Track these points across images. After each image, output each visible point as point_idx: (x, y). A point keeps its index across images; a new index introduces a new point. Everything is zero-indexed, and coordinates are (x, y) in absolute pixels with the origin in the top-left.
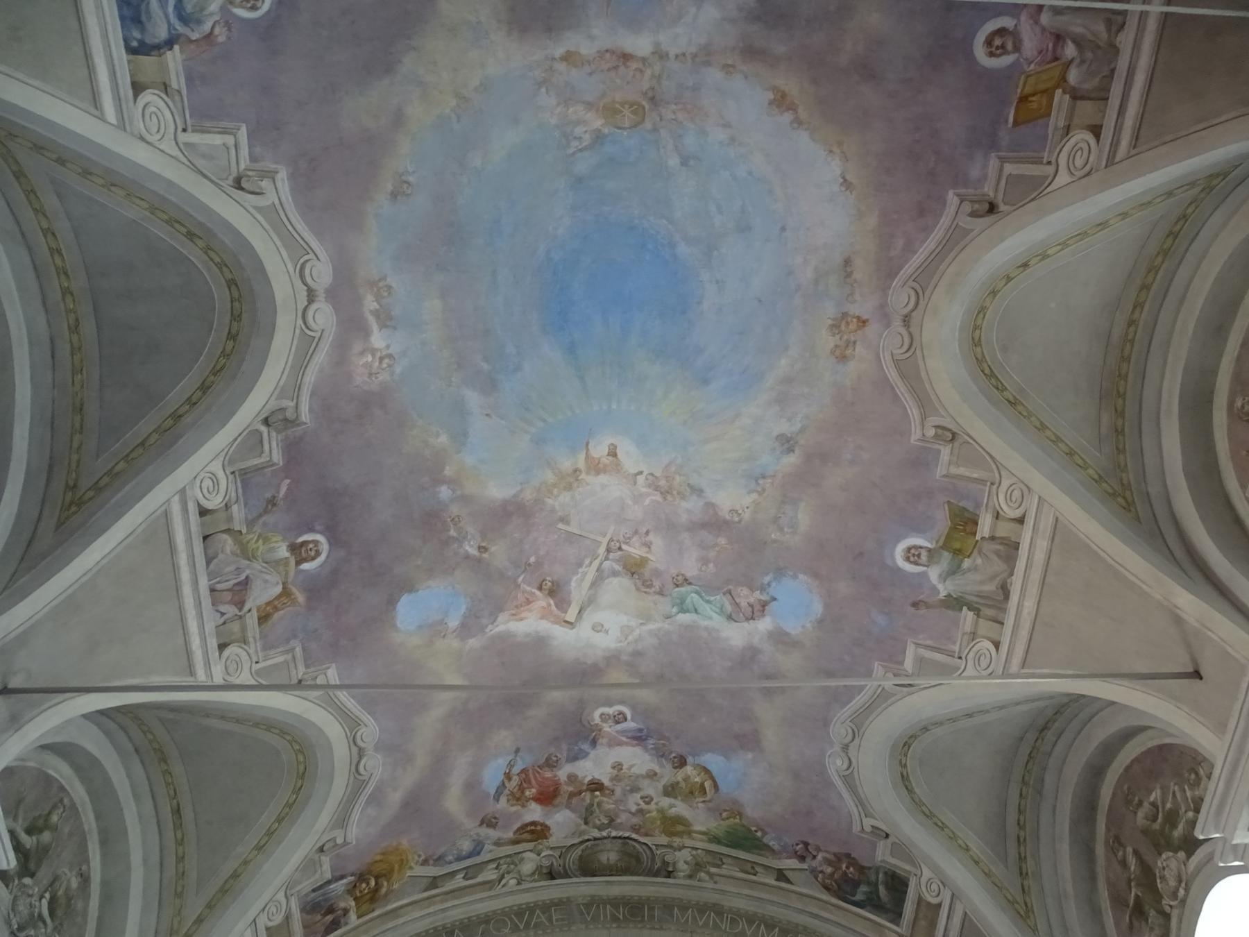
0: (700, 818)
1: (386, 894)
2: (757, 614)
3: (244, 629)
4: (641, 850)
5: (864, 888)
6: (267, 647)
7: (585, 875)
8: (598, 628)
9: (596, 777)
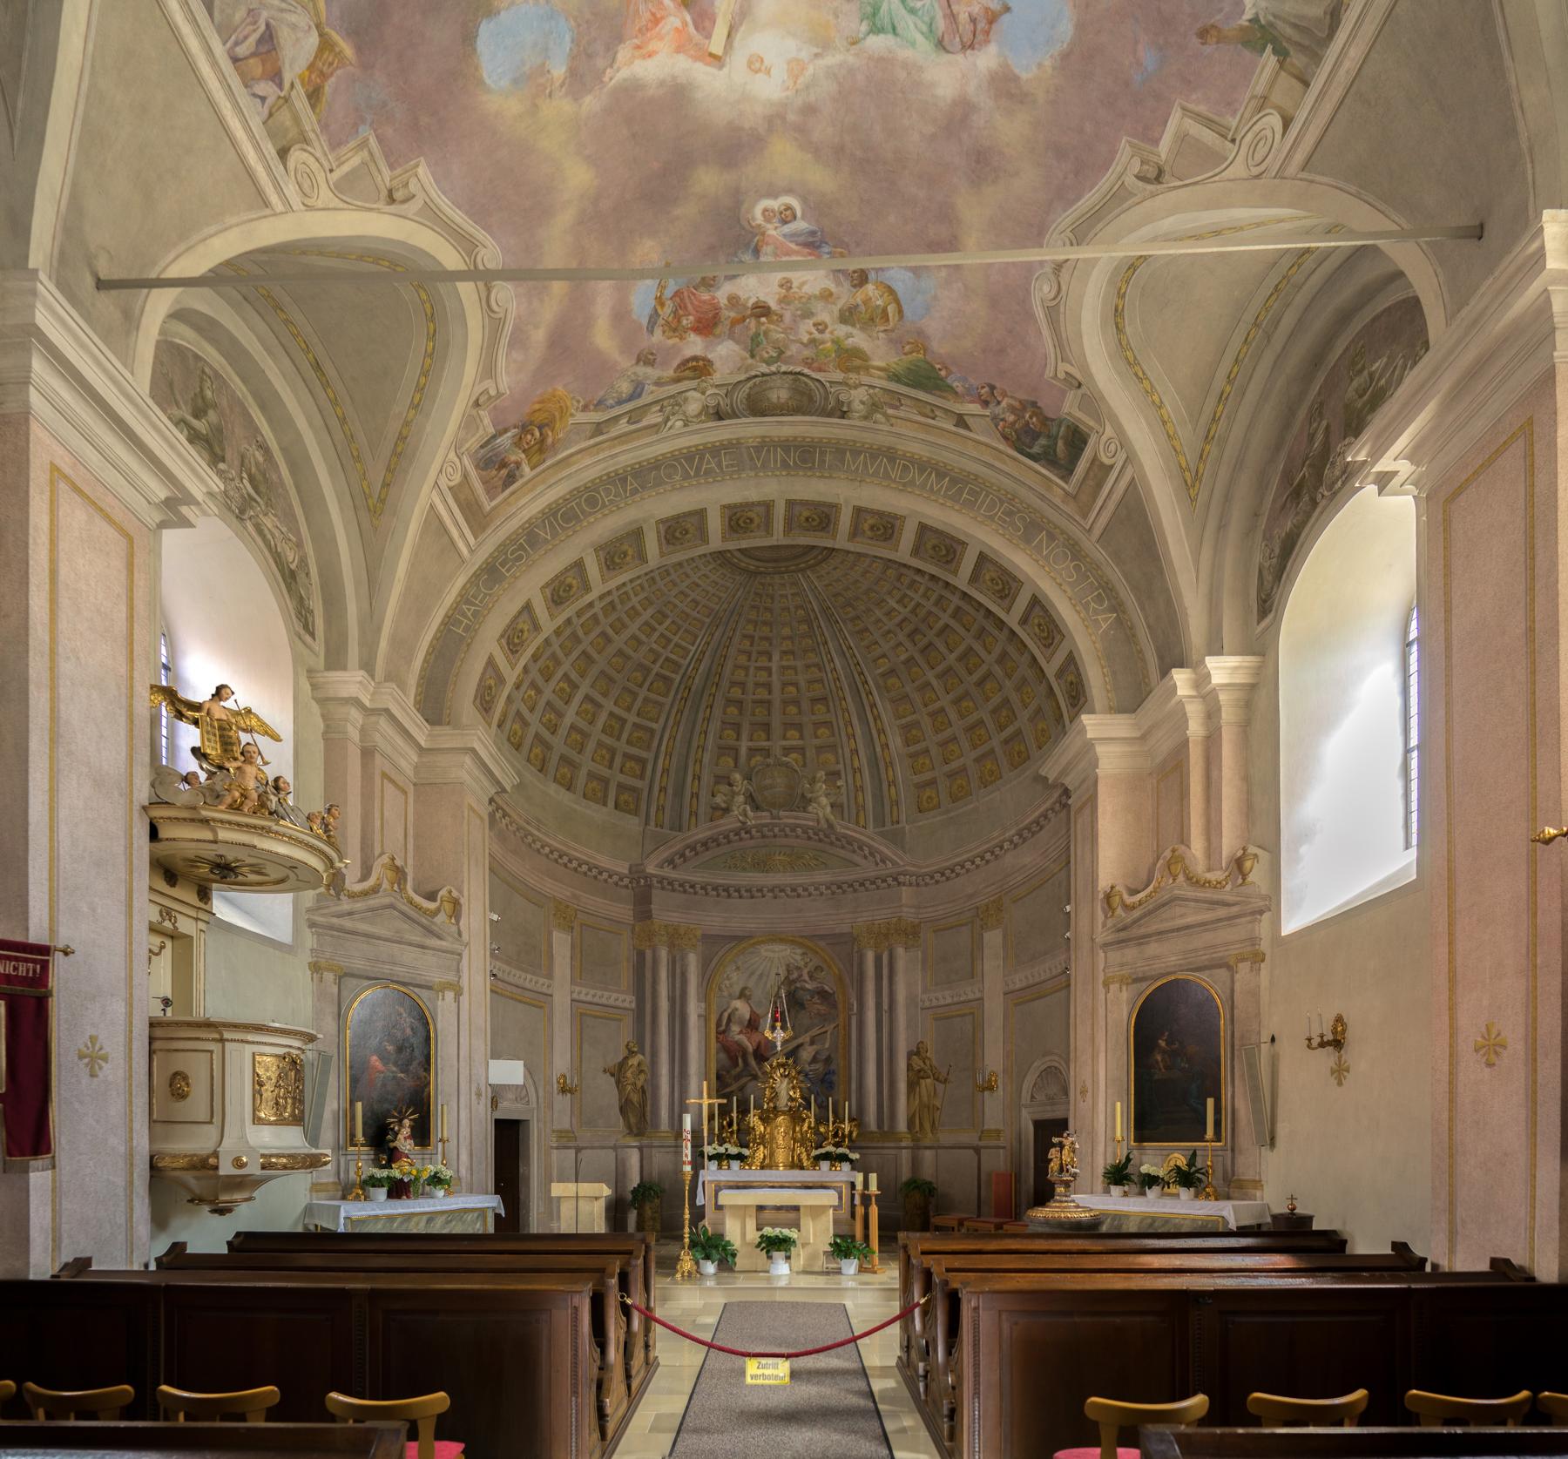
0: (879, 351)
1: (553, 444)
2: (980, 37)
5: (1043, 441)
6: (335, 145)
7: (755, 415)
8: (756, 65)
9: (762, 299)
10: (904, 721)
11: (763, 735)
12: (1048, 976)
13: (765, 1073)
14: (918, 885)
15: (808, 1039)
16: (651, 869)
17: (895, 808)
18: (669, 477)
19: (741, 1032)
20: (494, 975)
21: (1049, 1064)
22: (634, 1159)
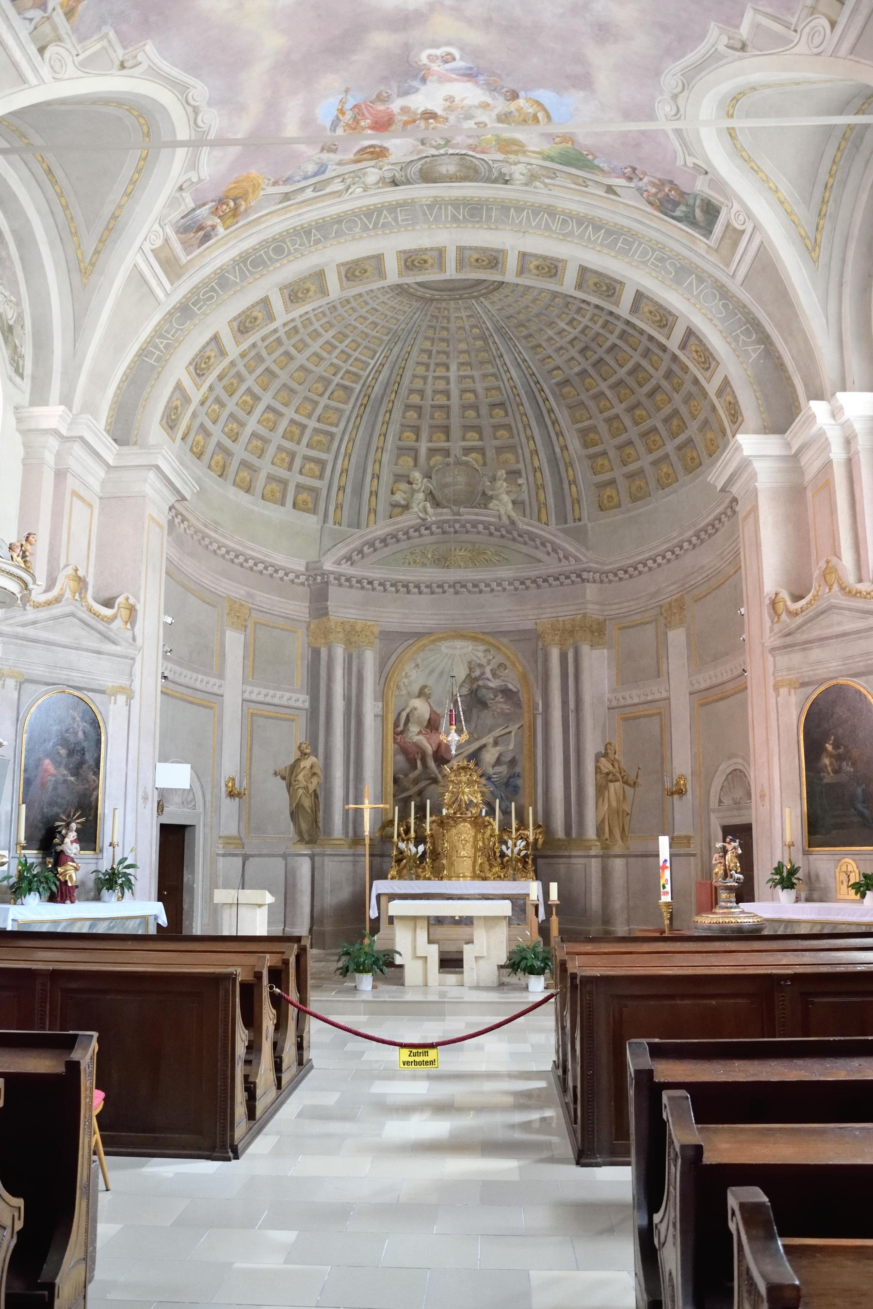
1: (246, 210)
3: (55, 28)
4: (478, 163)
5: (682, 208)
6: (82, 39)
10: (580, 425)
11: (443, 437)
12: (729, 676)
13: (444, 776)
14: (602, 582)
15: (491, 740)
16: (328, 566)
17: (576, 505)
18: (350, 229)
19: (420, 733)
20: (165, 677)
22: (304, 867)
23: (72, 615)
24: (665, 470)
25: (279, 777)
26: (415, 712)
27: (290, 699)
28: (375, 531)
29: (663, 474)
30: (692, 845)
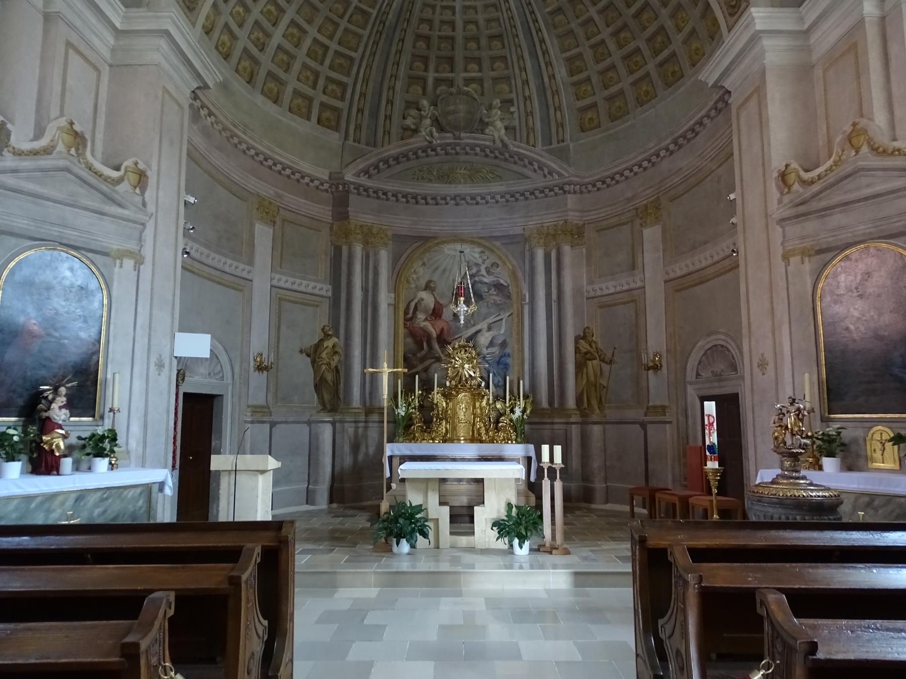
10: (568, 54)
11: (447, 67)
13: (449, 355)
14: (581, 192)
15: (485, 326)
16: (349, 177)
17: (560, 129)
19: (426, 319)
21: (714, 343)
22: (326, 433)
23: (67, 170)
24: (644, 88)
25: (304, 354)
26: (422, 302)
27: (315, 288)
28: (389, 150)
29: (642, 93)
30: (667, 414)
